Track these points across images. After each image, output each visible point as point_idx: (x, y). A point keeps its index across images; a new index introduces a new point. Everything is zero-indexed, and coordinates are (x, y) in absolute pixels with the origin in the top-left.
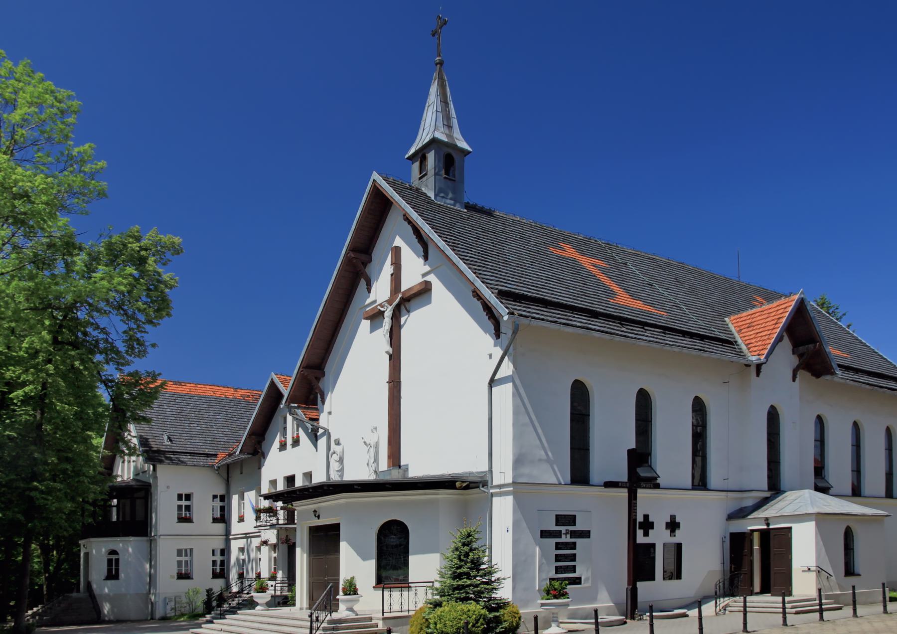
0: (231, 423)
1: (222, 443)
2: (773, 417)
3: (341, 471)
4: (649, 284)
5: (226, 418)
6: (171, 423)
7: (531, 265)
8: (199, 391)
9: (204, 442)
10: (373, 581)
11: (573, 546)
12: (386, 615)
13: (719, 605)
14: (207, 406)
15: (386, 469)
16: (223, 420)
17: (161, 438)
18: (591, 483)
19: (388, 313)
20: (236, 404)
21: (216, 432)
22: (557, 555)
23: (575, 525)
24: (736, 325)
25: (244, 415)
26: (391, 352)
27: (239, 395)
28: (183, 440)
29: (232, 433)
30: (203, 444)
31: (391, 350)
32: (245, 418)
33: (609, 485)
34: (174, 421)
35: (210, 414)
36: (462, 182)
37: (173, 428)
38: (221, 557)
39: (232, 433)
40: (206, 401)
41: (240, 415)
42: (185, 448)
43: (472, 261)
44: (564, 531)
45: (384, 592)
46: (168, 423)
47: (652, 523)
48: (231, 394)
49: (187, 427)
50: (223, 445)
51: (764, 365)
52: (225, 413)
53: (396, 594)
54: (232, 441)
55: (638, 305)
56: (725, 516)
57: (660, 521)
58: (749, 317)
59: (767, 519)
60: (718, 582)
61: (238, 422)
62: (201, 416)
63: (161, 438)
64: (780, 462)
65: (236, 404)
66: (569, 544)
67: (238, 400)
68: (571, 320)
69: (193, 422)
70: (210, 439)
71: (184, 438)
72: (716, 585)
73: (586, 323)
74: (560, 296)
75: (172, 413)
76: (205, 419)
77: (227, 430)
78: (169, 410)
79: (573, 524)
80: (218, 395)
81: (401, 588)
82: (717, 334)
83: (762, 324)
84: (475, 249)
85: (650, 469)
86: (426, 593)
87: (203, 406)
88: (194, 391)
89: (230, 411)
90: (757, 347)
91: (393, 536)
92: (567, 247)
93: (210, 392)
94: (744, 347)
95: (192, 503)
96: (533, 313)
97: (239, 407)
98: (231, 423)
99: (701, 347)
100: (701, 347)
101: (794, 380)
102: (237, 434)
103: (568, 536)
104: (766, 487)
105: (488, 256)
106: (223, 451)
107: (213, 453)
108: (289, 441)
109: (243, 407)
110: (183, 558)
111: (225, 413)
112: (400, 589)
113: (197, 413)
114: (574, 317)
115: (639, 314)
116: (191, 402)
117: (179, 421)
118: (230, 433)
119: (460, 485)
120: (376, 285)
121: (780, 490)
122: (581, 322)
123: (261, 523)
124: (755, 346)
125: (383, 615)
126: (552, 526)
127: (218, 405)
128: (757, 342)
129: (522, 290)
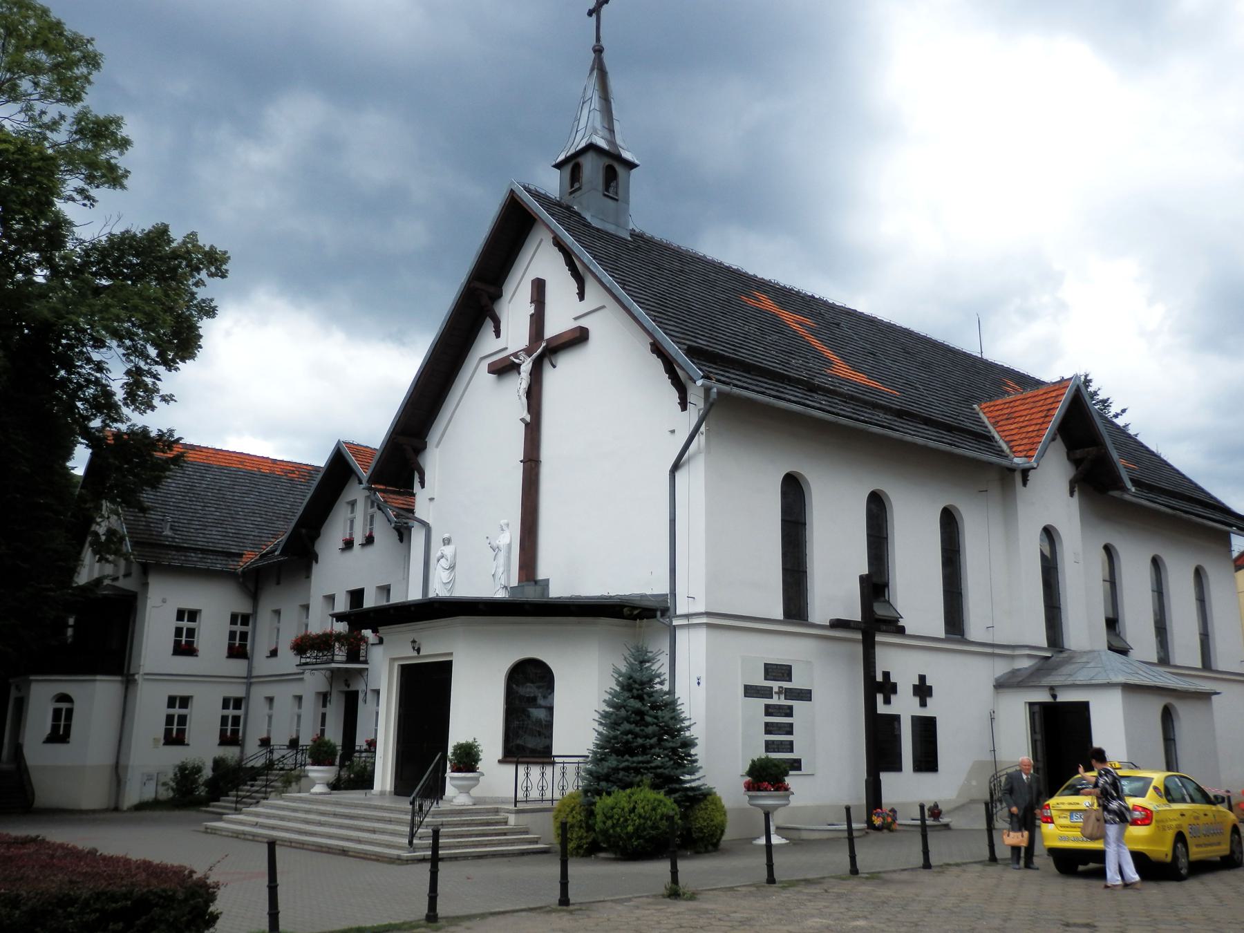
0: (265, 509)
1: (251, 537)
3: (452, 582)
4: (871, 354)
5: (259, 501)
6: (175, 504)
7: (723, 316)
8: (220, 460)
9: (224, 534)
10: (499, 754)
11: (789, 712)
13: (996, 814)
14: (232, 483)
15: (517, 585)
16: (254, 504)
17: (160, 526)
18: (810, 620)
19: (526, 366)
20: (274, 482)
21: (243, 521)
22: (767, 724)
23: (790, 680)
24: (988, 415)
25: (285, 499)
27: (279, 470)
28: (192, 530)
29: (266, 524)
30: (223, 538)
31: (528, 418)
32: (287, 502)
33: (838, 624)
34: (181, 501)
35: (236, 494)
36: (627, 202)
37: (178, 511)
39: (266, 524)
40: (229, 475)
41: (279, 498)
42: (195, 543)
43: (649, 305)
44: (776, 689)
46: (171, 504)
48: (267, 468)
49: (200, 512)
50: (251, 540)
51: (1032, 471)
52: (257, 494)
53: (535, 771)
54: (266, 535)
55: (861, 378)
56: (991, 683)
57: (905, 682)
58: (1007, 405)
59: (1052, 688)
60: (993, 779)
61: (276, 508)
62: (221, 496)
63: (160, 526)
64: (1060, 608)
65: (274, 482)
66: (782, 709)
67: (278, 476)
68: (782, 392)
69: (209, 505)
70: (233, 531)
71: (194, 527)
72: (990, 782)
73: (802, 398)
74: (763, 359)
75: (178, 489)
76: (227, 500)
77: (259, 519)
78: (174, 485)
79: (788, 679)
80: (249, 468)
82: (968, 424)
83: (1026, 416)
84: (650, 290)
85: (888, 605)
87: (225, 482)
88: (214, 459)
89: (265, 492)
90: (1023, 446)
91: (529, 684)
92: (762, 297)
93: (236, 462)
94: (1005, 446)
95: (199, 625)
96: (734, 379)
97: (278, 486)
98: (265, 509)
99: (951, 440)
100: (951, 440)
101: (1072, 494)
102: (273, 525)
103: (782, 697)
104: (1044, 644)
105: (667, 300)
106: (252, 549)
107: (237, 551)
108: (358, 539)
109: (285, 488)
110: (177, 711)
111: (257, 494)
113: (216, 491)
114: (785, 388)
115: (866, 392)
116: (207, 476)
117: (188, 502)
118: (264, 524)
119: (629, 612)
121: (1063, 648)
122: (796, 396)
123: (308, 660)
124: (1020, 445)
125: (515, 806)
126: (759, 680)
127: (247, 481)
129: (716, 348)
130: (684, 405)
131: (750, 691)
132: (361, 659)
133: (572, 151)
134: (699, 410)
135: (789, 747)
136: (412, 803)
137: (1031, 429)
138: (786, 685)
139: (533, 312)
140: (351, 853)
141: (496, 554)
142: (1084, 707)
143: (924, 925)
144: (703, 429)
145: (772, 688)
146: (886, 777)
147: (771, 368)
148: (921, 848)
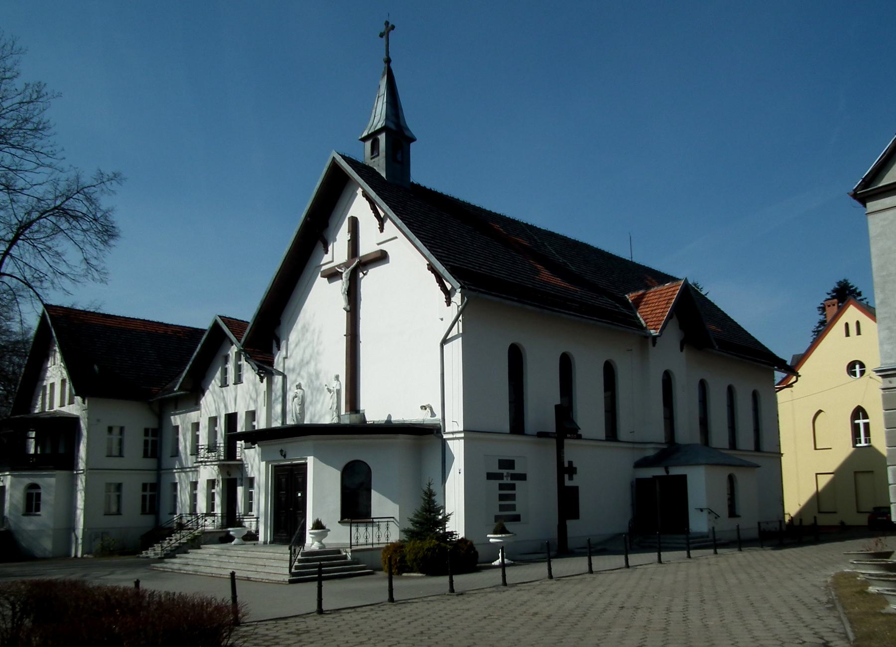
2: (667, 381)
11: (513, 487)
12: (354, 548)
26: (348, 308)
33: (541, 435)
38: (39, 492)
45: (352, 528)
47: (576, 468)
53: (362, 529)
81: (367, 524)
86: (388, 528)
101: (682, 350)
103: (509, 478)
112: (356, 524)
120: (333, 245)
124: (651, 321)
126: (495, 469)
128: (653, 318)
130: (449, 302)
131: (490, 476)
132: (238, 458)
133: (372, 131)
134: (458, 306)
135: (513, 507)
136: (290, 549)
137: (658, 311)
138: (511, 471)
139: (349, 238)
140: (252, 579)
141: (332, 396)
142: (684, 478)
143: (105, 273)
144: (460, 318)
145: (503, 474)
146: (570, 523)
147: (501, 278)
148: (588, 562)
